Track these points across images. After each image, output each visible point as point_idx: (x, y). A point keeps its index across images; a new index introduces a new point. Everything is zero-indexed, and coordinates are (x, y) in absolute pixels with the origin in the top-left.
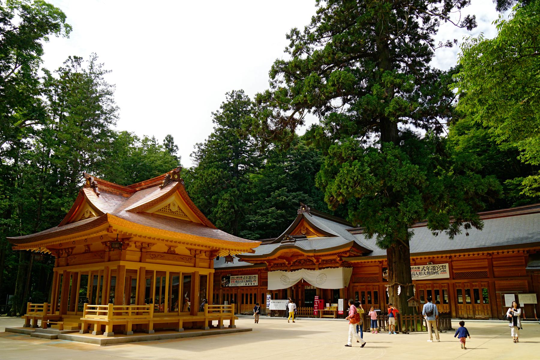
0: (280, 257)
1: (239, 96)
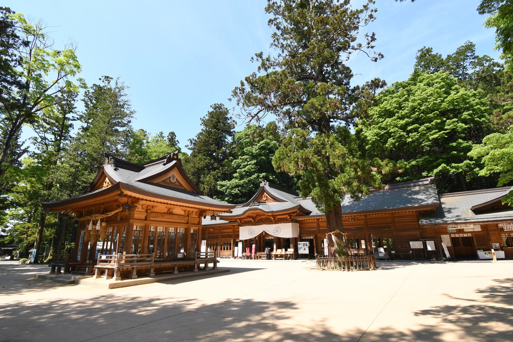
0: (249, 217)
1: (220, 108)
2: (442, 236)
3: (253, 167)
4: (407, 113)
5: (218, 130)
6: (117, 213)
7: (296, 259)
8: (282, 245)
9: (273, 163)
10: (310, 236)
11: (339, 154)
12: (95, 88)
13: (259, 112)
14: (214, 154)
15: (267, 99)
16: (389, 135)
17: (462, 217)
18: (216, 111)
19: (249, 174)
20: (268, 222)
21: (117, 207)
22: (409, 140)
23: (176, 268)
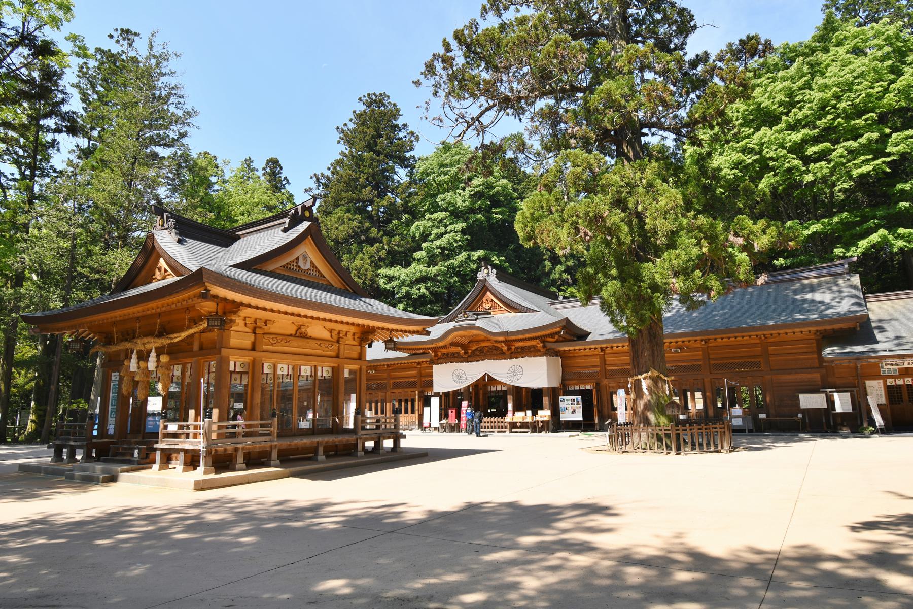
0: (454, 344)
1: (380, 103)
2: (869, 383)
3: (458, 238)
4: (807, 116)
5: (378, 154)
6: (192, 335)
7: (555, 430)
8: (525, 402)
9: (517, 227)
10: (585, 383)
11: (667, 208)
12: (99, 57)
13: (482, 114)
14: (370, 208)
15: (501, 81)
16: (764, 167)
17: (905, 340)
18: (373, 111)
19: (448, 252)
20: (495, 355)
21: (192, 320)
22: (809, 178)
23: (321, 450)
